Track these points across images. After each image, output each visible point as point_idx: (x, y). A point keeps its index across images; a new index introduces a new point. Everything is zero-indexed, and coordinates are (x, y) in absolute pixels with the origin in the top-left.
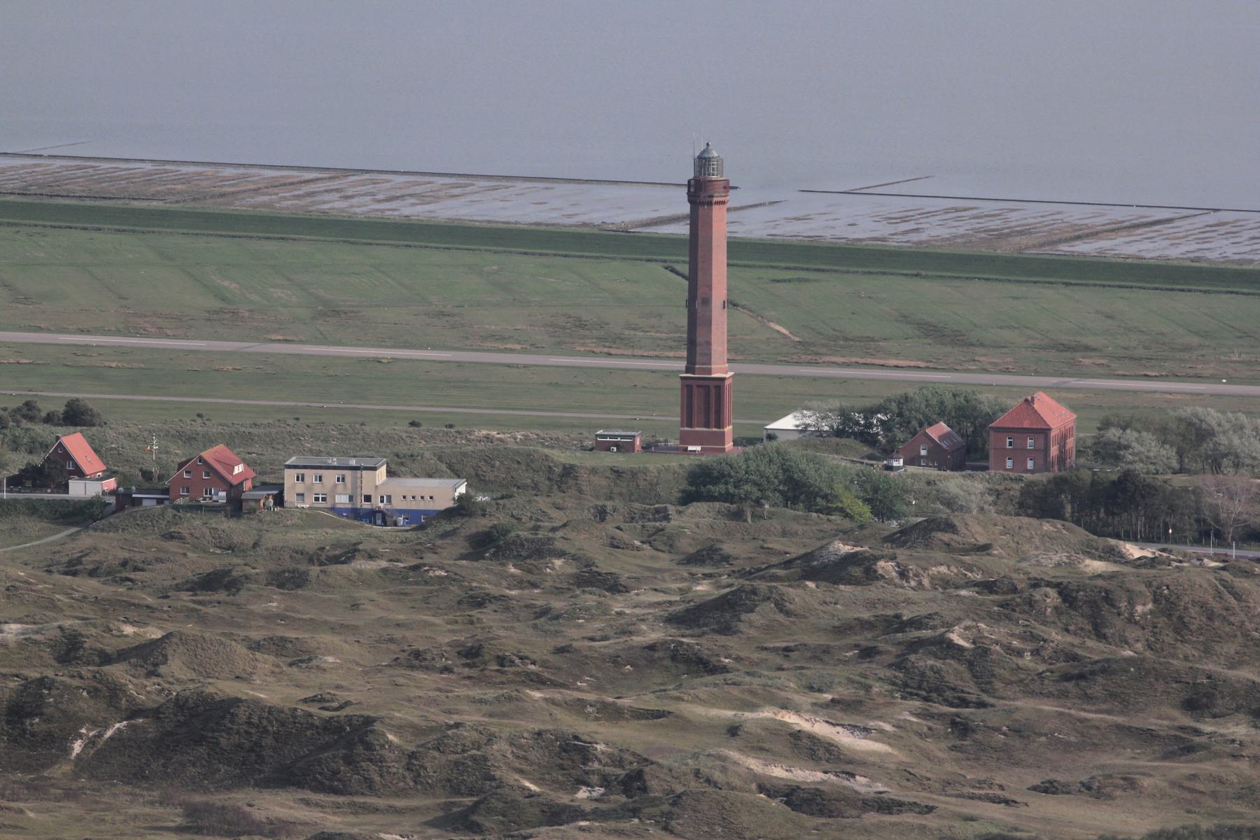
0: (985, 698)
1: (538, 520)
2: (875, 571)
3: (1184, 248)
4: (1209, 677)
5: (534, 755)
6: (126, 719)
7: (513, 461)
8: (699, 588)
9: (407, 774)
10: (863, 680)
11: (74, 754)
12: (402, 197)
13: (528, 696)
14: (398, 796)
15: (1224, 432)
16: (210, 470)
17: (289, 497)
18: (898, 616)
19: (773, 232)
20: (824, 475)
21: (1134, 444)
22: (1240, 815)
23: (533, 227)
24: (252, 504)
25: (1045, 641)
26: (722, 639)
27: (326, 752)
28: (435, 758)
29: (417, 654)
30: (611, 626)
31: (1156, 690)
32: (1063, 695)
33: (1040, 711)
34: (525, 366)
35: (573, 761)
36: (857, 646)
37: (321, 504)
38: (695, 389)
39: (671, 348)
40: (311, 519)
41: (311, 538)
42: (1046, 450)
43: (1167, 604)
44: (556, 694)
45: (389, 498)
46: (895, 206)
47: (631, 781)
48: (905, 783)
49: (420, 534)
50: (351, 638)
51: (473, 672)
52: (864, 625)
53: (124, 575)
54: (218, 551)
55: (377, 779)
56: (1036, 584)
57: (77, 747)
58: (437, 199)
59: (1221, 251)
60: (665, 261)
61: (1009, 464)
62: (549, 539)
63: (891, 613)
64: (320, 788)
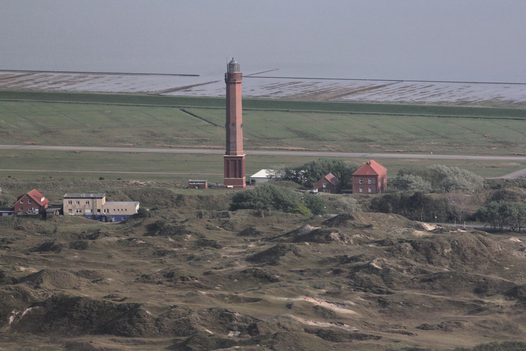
0: (390, 290)
1: (173, 218)
2: (330, 237)
3: (394, 97)
4: (484, 279)
5: (209, 318)
6: (31, 306)
7: (156, 193)
8: (251, 246)
9: (156, 327)
10: (337, 284)
11: (10, 322)
12: (60, 82)
13: (201, 293)
14: (153, 337)
15: (451, 175)
16: (31, 200)
17: (66, 211)
18: (346, 256)
19: (221, 94)
20: (291, 197)
21: (414, 181)
22: (506, 337)
23: (120, 94)
24: (50, 214)
25: (412, 265)
26: (273, 268)
27: (119, 319)
28: (167, 321)
29: (147, 277)
30: (223, 263)
31: (462, 285)
32: (423, 288)
33: (414, 295)
34: (137, 153)
35: (226, 320)
36: (331, 269)
37: (79, 213)
38: (230, 161)
39: (196, 144)
40: (76, 220)
41: (79, 228)
42: (376, 184)
43: (457, 248)
44: (209, 292)
45: (108, 210)
46: (268, 82)
47: (252, 329)
48: (364, 327)
49: (123, 225)
50: (115, 270)
51: (172, 284)
52: (331, 260)
53: (3, 245)
54: (39, 234)
55: (143, 330)
56: (401, 241)
57: (11, 319)
58: (75, 83)
59: (410, 98)
60: (179, 107)
61: (361, 190)
62: (183, 226)
63: (342, 255)
64: (119, 334)
